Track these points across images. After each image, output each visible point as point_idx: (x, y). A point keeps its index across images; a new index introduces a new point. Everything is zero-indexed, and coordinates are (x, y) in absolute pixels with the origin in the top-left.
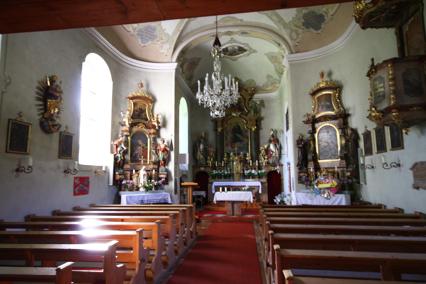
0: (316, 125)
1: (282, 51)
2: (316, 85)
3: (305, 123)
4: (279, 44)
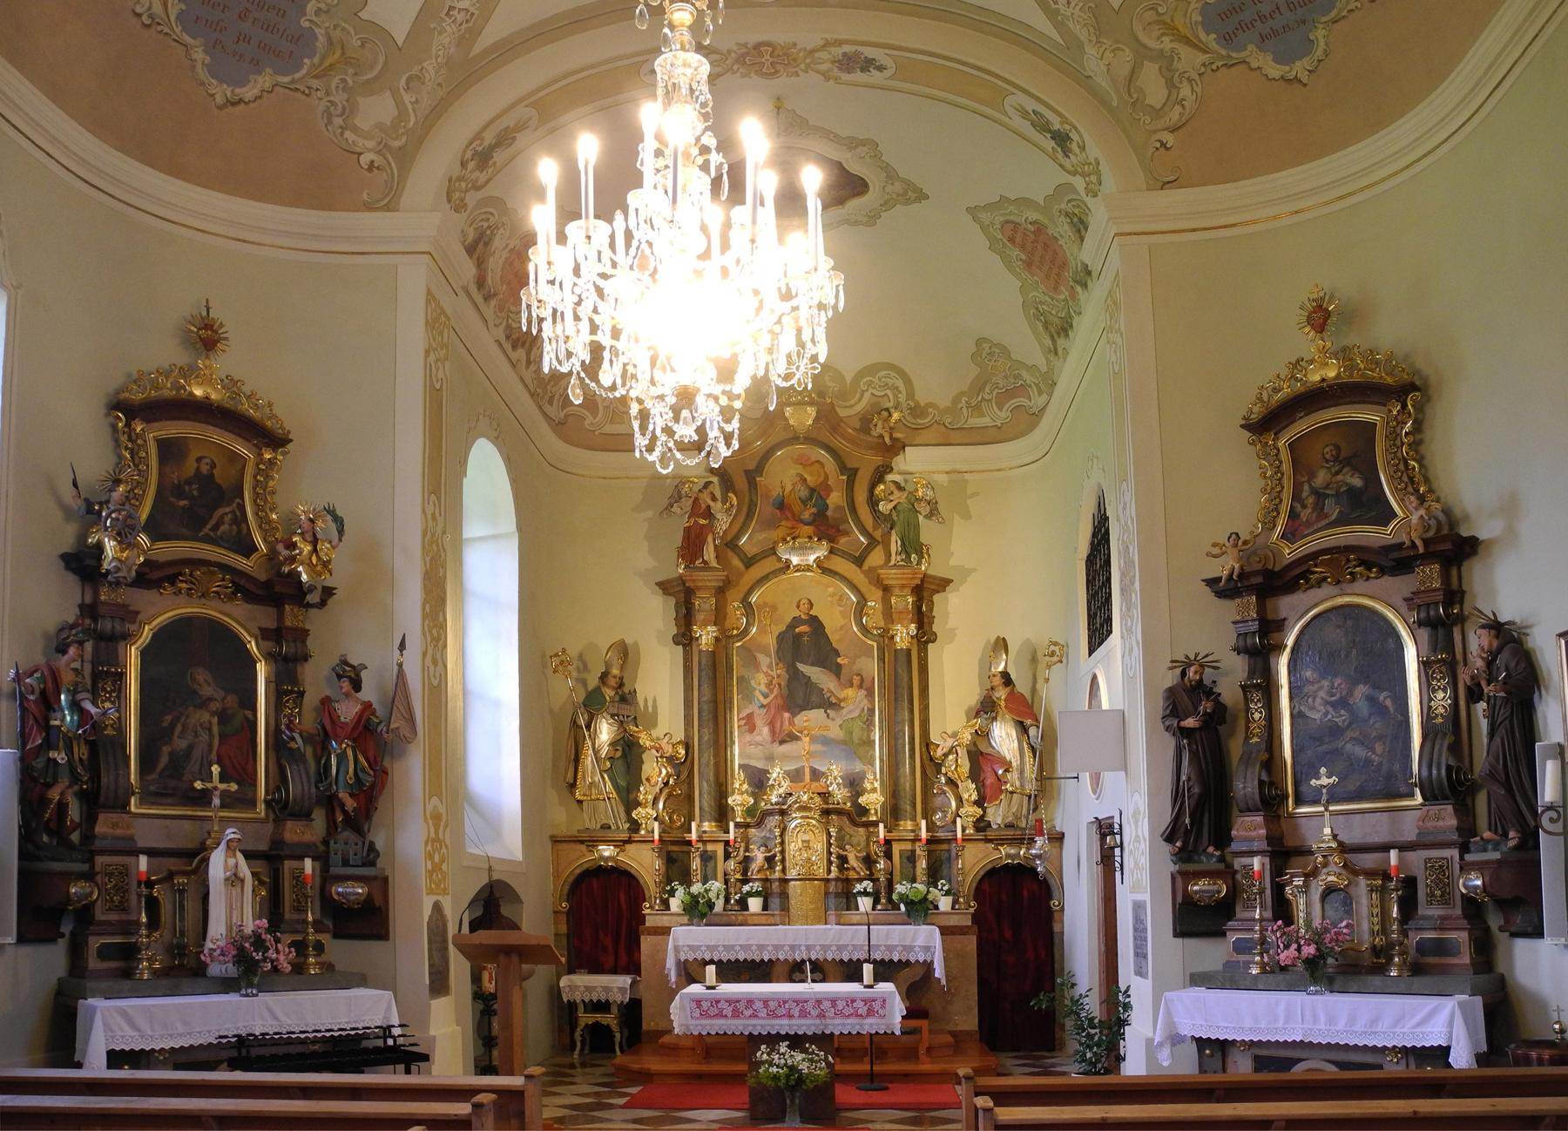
0: (1285, 605)
1: (1079, 183)
2: (1284, 373)
3: (1220, 594)
4: (1061, 139)
